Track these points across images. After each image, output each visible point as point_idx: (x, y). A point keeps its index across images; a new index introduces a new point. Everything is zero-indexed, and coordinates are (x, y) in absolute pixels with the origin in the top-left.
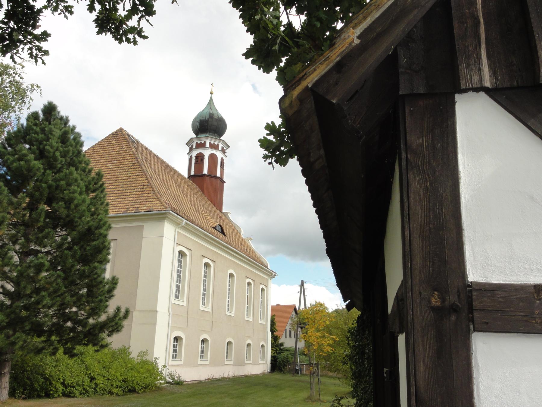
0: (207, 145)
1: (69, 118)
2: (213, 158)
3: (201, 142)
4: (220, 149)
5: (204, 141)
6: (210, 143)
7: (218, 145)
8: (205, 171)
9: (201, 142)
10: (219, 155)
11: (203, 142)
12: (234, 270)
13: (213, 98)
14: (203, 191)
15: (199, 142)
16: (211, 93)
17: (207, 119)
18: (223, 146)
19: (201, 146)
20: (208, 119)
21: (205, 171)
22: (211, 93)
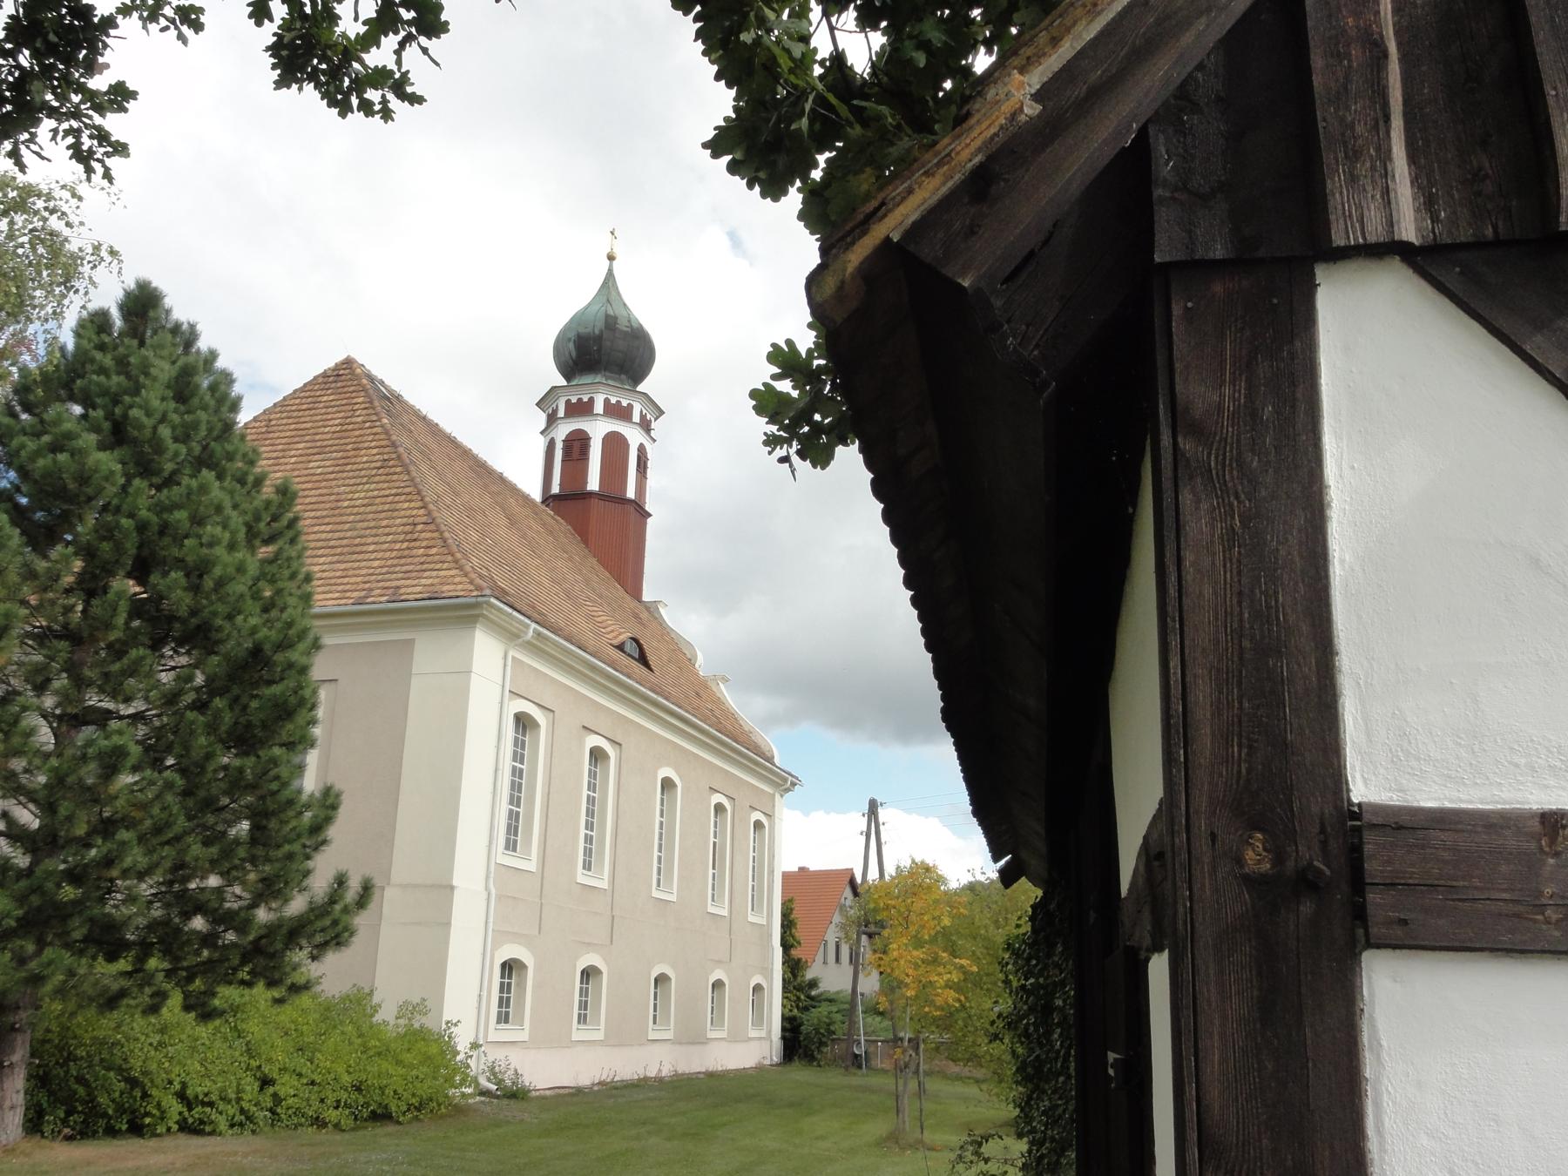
0: (599, 407)
1: (710, 134)
2: (615, 444)
3: (580, 400)
4: (636, 418)
5: (589, 396)
6: (607, 401)
7: (630, 407)
8: (593, 484)
9: (580, 400)
10: (634, 436)
11: (625, 403)
12: (677, 772)
13: (616, 272)
14: (585, 541)
15: (574, 400)
16: (611, 258)
17: (597, 332)
18: (644, 411)
19: (581, 409)
20: (601, 331)
21: (593, 484)
22: (611, 258)
